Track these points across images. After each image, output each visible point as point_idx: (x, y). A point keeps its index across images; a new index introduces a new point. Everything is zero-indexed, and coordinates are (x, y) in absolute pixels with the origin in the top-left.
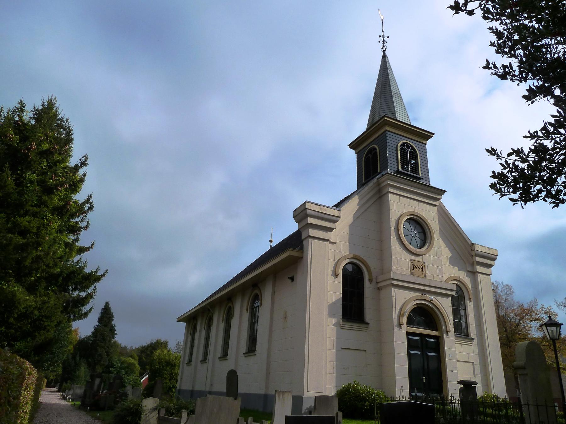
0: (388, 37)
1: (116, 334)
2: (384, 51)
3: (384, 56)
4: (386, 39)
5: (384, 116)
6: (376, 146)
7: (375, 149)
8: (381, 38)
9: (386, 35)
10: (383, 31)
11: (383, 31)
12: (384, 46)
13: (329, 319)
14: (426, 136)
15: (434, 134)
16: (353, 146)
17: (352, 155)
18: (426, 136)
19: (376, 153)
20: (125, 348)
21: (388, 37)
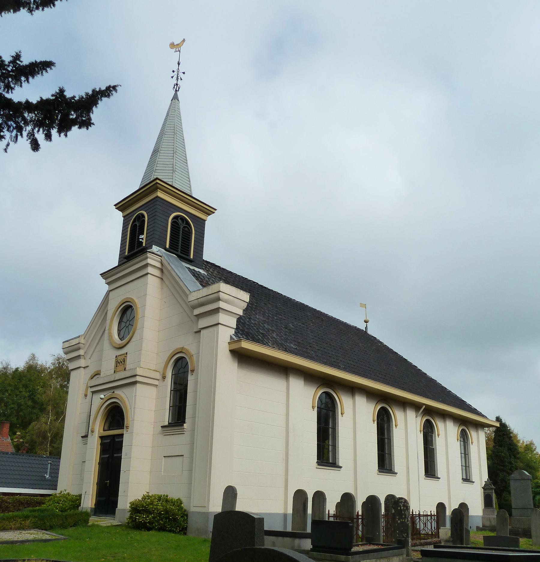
0: (184, 73)
1: (87, 129)
2: (176, 91)
3: (175, 97)
4: (181, 75)
5: (157, 179)
6: (145, 213)
7: (143, 216)
8: (176, 73)
9: (181, 70)
10: (179, 64)
11: (179, 64)
12: (177, 84)
13: (482, 536)
14: (209, 211)
15: (216, 210)
16: (122, 206)
17: (119, 216)
18: (209, 211)
19: (144, 221)
20: (20, 103)
21: (184, 73)
